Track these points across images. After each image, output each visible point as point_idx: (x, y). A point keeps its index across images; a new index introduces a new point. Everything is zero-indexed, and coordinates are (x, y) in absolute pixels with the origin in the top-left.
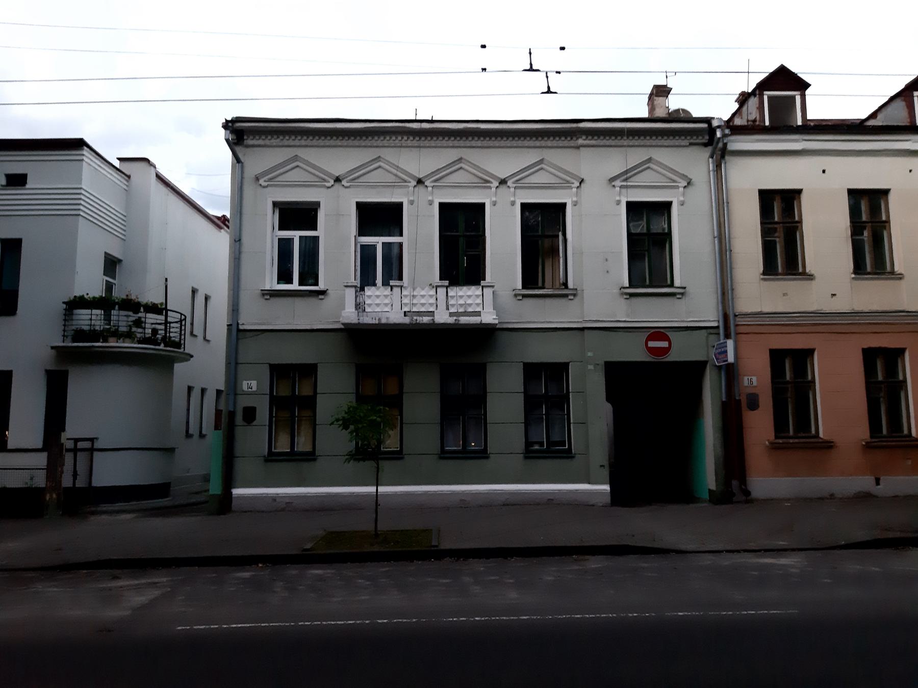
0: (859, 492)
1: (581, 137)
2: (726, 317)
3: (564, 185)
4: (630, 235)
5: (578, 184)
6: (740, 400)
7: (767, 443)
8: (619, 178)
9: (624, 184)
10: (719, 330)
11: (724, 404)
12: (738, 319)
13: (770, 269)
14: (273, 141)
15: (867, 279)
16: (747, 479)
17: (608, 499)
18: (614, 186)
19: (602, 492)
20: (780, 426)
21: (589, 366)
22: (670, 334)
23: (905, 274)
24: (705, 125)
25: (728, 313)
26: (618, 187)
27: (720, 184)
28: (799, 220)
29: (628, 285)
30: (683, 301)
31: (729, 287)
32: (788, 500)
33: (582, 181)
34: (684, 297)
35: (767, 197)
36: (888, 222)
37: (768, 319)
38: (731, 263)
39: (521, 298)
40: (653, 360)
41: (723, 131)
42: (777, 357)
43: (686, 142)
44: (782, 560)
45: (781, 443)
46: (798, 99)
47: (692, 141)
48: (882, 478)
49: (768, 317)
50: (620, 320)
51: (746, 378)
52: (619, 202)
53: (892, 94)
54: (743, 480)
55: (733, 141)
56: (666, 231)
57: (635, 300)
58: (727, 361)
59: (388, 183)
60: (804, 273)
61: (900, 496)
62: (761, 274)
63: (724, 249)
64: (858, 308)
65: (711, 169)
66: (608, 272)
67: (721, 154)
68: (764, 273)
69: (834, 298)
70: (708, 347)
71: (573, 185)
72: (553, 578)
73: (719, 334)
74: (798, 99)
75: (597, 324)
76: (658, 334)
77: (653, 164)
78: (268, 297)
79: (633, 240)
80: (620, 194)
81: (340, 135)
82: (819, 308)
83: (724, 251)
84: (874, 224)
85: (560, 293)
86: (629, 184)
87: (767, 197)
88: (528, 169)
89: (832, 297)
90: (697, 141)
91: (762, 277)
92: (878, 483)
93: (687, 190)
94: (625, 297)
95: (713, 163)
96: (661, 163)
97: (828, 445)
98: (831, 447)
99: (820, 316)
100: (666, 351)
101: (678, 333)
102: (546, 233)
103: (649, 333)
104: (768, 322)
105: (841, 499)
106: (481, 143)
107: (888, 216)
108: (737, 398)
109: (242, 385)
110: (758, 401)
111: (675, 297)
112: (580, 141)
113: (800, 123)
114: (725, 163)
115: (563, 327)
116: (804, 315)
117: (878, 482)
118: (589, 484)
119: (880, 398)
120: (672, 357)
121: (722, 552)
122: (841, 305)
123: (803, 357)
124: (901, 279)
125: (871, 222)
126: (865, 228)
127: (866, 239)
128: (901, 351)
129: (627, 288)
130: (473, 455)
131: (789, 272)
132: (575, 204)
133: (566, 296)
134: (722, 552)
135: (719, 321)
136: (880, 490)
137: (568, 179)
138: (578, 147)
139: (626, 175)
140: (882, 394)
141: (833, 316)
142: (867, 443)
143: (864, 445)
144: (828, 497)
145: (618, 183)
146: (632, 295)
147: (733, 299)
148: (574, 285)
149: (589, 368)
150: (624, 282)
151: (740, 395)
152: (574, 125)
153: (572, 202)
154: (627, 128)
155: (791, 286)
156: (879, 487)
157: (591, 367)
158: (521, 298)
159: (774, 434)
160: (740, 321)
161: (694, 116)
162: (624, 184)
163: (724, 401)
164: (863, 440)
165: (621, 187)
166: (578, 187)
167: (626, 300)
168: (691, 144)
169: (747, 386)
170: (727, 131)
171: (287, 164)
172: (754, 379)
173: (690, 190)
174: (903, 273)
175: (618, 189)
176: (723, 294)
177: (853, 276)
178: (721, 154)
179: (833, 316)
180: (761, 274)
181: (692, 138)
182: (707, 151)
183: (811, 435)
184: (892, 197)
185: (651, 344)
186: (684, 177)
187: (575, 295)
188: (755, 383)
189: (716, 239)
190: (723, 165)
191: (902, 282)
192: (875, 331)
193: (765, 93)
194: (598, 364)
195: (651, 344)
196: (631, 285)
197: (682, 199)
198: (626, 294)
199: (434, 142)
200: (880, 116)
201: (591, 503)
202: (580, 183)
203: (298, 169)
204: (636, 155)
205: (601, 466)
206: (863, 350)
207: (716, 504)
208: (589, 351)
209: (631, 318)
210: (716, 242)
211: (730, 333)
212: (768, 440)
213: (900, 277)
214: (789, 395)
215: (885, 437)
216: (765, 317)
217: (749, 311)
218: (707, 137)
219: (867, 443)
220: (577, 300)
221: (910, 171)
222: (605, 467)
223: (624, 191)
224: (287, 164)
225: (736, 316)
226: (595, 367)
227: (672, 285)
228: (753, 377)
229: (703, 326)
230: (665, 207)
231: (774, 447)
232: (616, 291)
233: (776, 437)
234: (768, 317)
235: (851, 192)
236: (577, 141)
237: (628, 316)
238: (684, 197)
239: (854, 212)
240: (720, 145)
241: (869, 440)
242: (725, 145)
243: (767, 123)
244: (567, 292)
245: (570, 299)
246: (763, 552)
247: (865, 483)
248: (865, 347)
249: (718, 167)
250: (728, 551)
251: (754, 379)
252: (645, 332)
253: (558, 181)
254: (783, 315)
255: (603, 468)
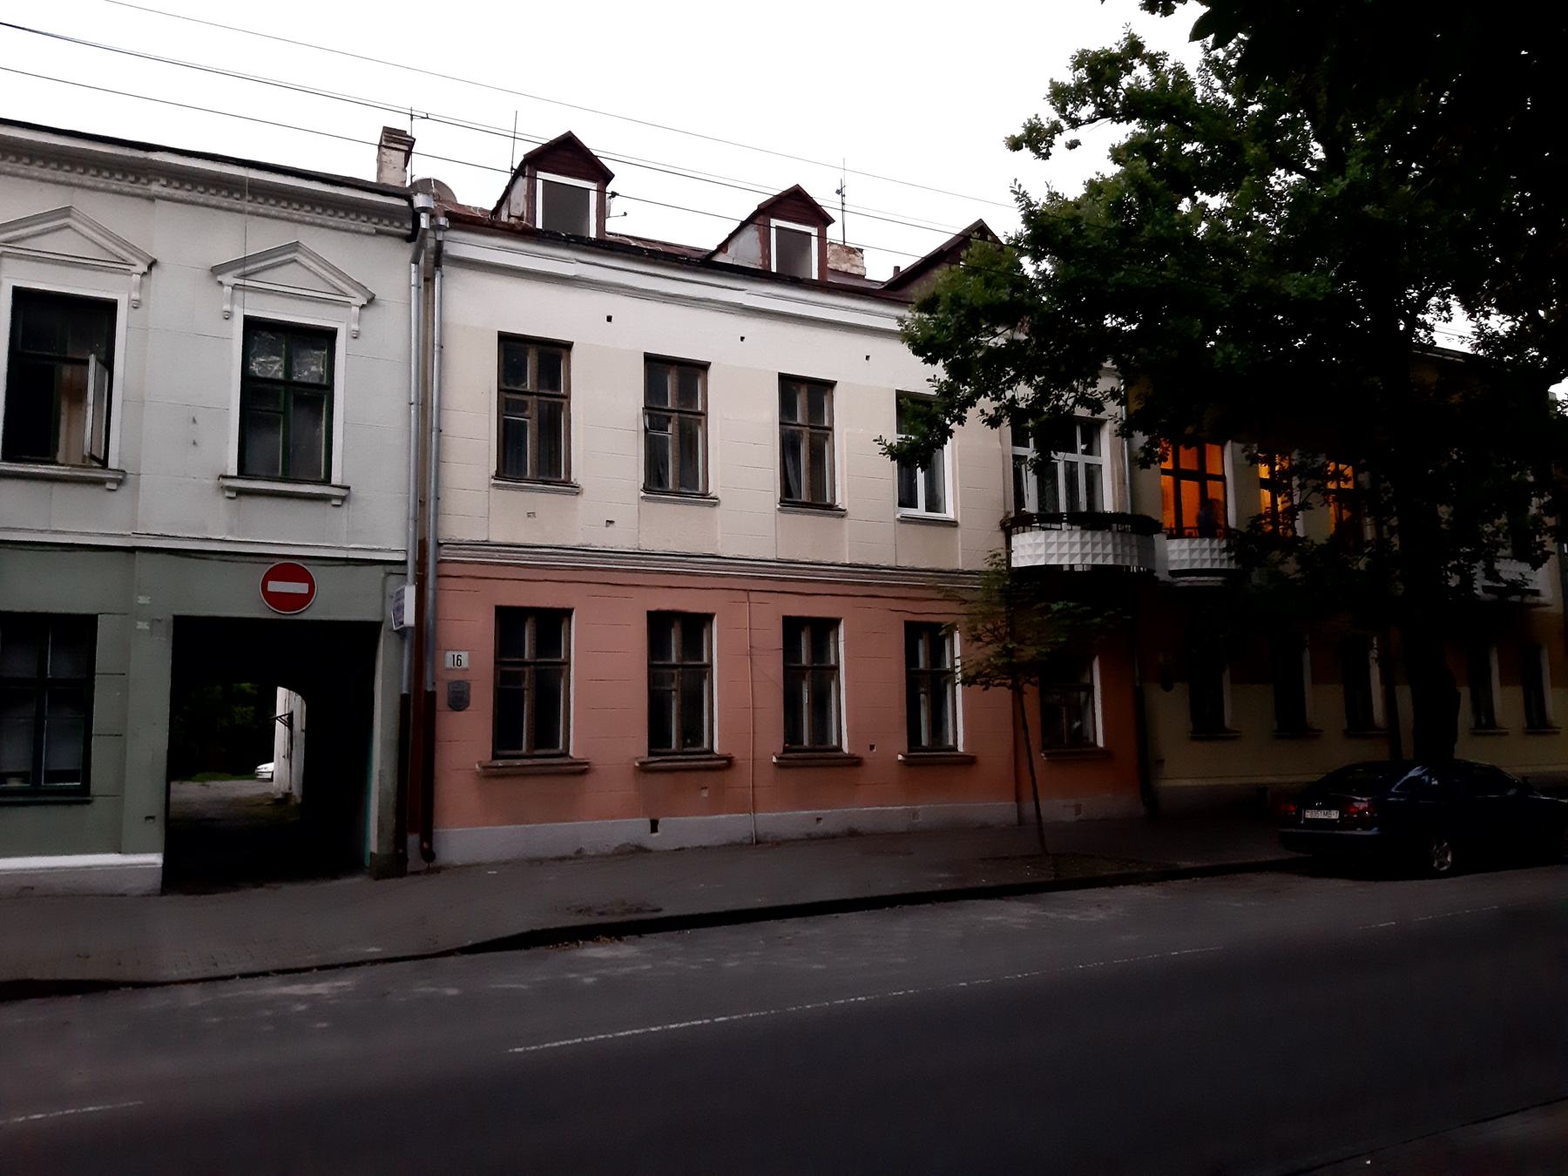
0: (623, 845)
1: (158, 181)
2: (422, 546)
3: (118, 266)
4: (247, 379)
5: (145, 269)
6: (433, 694)
7: (477, 766)
8: (231, 270)
9: (241, 282)
10: (407, 568)
11: (404, 699)
12: (443, 551)
13: (510, 467)
14: (86, 177)
15: (666, 501)
16: (434, 830)
17: (155, 881)
18: (220, 283)
19: (145, 869)
20: (505, 735)
21: (139, 623)
22: (313, 570)
23: (583, 486)
24: (405, 203)
25: (427, 539)
26: (229, 286)
27: (430, 312)
28: (566, 394)
29: (235, 474)
30: (343, 511)
31: (432, 495)
32: (492, 865)
33: (153, 264)
34: (345, 505)
35: (512, 347)
36: (704, 414)
37: (497, 555)
38: (438, 453)
39: (339, 503)
40: (275, 616)
41: (433, 216)
42: (509, 620)
43: (368, 227)
44: (317, 986)
45: (500, 767)
46: (593, 197)
47: (380, 227)
48: (661, 820)
49: (498, 551)
50: (213, 537)
51: (449, 655)
52: (228, 316)
53: (744, 218)
54: (427, 834)
55: (453, 241)
56: (325, 382)
57: (247, 502)
58: (402, 623)
59: (67, 256)
60: (567, 483)
61: (688, 848)
62: (493, 477)
63: (429, 427)
64: (647, 545)
65: (413, 283)
66: (195, 443)
67: (434, 263)
68: (498, 476)
69: (611, 527)
70: (384, 598)
71: (133, 269)
72: (595, 979)
73: (405, 574)
74: (593, 197)
75: (160, 542)
76: (290, 568)
77: (301, 253)
78: (234, 495)
79: (252, 388)
80: (232, 301)
81: (306, 203)
82: (585, 543)
83: (428, 431)
84: (681, 415)
85: (82, 474)
86: (247, 283)
87: (512, 347)
88: (34, 221)
89: (607, 526)
90: (391, 229)
91: (493, 481)
92: (654, 828)
93: (367, 313)
94: (228, 494)
95: (418, 272)
96: (314, 254)
97: (581, 770)
98: (584, 772)
99: (584, 556)
100: (301, 601)
101: (72, 554)
102: (69, 355)
103: (272, 566)
104: (497, 558)
105: (593, 857)
106: (79, 178)
107: (705, 406)
108: (429, 689)
109: (444, 657)
110: (469, 695)
111: (102, 487)
112: (155, 188)
113: (593, 234)
114: (442, 276)
115: (70, 541)
116: (557, 551)
117: (654, 826)
118: (120, 853)
119: (671, 691)
120: (312, 613)
121: (233, 977)
122: (619, 539)
123: (553, 622)
124: (715, 505)
125: (811, 427)
126: (669, 419)
127: (670, 437)
128: (834, 623)
129: (232, 477)
130: (21, 799)
131: (541, 478)
132: (136, 305)
133: (100, 482)
134: (233, 977)
135: (406, 552)
136: (659, 841)
137: (125, 254)
138: (151, 199)
139: (246, 267)
140: (674, 686)
141: (620, 558)
142: (642, 764)
143: (478, 773)
144: (572, 854)
145: (229, 279)
146: (241, 492)
147: (436, 515)
148: (120, 462)
149: (138, 627)
150: (227, 466)
151: (434, 684)
152: (141, 154)
153: (130, 300)
154: (250, 179)
155: (543, 501)
156: (655, 835)
157: (143, 625)
158: (234, 495)
159: (491, 750)
160: (445, 554)
161: (460, 201)
162: (241, 282)
163: (405, 694)
164: (637, 758)
165: (234, 287)
166: (144, 274)
167: (230, 501)
168: (379, 233)
169: (451, 669)
170: (443, 221)
171: (279, 253)
172: (465, 656)
173: (369, 314)
174: (719, 496)
175: (228, 290)
176: (422, 503)
177: (643, 494)
178: (434, 263)
179: (620, 558)
180: (493, 477)
181: (380, 221)
182: (407, 250)
183: (703, 750)
184: (838, 392)
185: (275, 586)
186: (361, 288)
187: (120, 482)
188: (465, 664)
189: (413, 406)
190: (437, 280)
191: (717, 510)
192: (561, 579)
193: (541, 175)
194: (159, 621)
195: (275, 586)
196: (243, 472)
197: (355, 327)
198: (229, 489)
199: (50, 171)
200: (731, 249)
201: (121, 891)
202: (150, 267)
203: (69, 230)
204: (266, 234)
205: (148, 818)
206: (650, 614)
207: (377, 879)
208: (141, 594)
209: (239, 537)
210: (412, 412)
211: (428, 575)
212: (479, 763)
213: (841, 514)
214: (526, 684)
215: (674, 753)
216: (493, 551)
217: (467, 538)
218: (410, 226)
219: (642, 764)
220: (124, 490)
221: (742, 339)
222: (157, 818)
223: (239, 294)
224: (279, 253)
225: (440, 545)
226: (151, 626)
227: (327, 481)
228: (461, 653)
229: (157, 546)
230: (324, 338)
231: (489, 774)
232: (212, 482)
233: (495, 757)
234: (498, 551)
235: (651, 360)
236: (148, 187)
237: (231, 532)
238: (359, 324)
239: (787, 406)
240: (431, 243)
241: (646, 758)
242: (439, 244)
243: (539, 225)
244: (103, 476)
245: (334, 506)
246: (315, 970)
247: (633, 829)
248: (653, 608)
249: (429, 280)
250: (244, 976)
251: (465, 656)
252: (266, 563)
253: (321, 286)
254: (515, 549)
255: (151, 821)
